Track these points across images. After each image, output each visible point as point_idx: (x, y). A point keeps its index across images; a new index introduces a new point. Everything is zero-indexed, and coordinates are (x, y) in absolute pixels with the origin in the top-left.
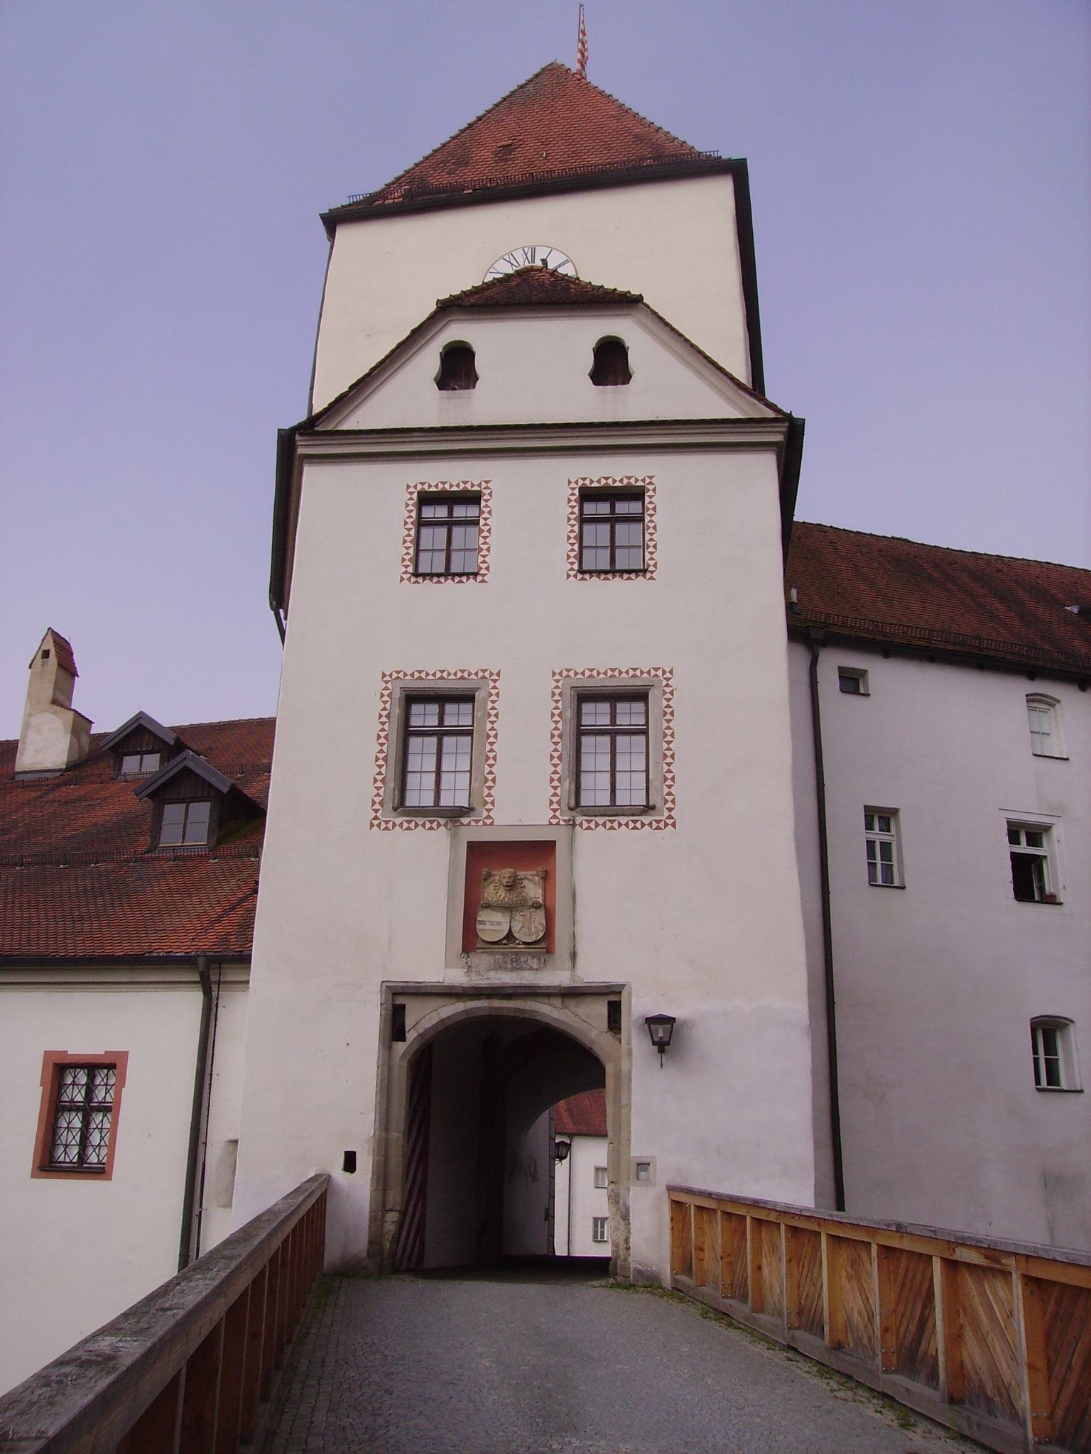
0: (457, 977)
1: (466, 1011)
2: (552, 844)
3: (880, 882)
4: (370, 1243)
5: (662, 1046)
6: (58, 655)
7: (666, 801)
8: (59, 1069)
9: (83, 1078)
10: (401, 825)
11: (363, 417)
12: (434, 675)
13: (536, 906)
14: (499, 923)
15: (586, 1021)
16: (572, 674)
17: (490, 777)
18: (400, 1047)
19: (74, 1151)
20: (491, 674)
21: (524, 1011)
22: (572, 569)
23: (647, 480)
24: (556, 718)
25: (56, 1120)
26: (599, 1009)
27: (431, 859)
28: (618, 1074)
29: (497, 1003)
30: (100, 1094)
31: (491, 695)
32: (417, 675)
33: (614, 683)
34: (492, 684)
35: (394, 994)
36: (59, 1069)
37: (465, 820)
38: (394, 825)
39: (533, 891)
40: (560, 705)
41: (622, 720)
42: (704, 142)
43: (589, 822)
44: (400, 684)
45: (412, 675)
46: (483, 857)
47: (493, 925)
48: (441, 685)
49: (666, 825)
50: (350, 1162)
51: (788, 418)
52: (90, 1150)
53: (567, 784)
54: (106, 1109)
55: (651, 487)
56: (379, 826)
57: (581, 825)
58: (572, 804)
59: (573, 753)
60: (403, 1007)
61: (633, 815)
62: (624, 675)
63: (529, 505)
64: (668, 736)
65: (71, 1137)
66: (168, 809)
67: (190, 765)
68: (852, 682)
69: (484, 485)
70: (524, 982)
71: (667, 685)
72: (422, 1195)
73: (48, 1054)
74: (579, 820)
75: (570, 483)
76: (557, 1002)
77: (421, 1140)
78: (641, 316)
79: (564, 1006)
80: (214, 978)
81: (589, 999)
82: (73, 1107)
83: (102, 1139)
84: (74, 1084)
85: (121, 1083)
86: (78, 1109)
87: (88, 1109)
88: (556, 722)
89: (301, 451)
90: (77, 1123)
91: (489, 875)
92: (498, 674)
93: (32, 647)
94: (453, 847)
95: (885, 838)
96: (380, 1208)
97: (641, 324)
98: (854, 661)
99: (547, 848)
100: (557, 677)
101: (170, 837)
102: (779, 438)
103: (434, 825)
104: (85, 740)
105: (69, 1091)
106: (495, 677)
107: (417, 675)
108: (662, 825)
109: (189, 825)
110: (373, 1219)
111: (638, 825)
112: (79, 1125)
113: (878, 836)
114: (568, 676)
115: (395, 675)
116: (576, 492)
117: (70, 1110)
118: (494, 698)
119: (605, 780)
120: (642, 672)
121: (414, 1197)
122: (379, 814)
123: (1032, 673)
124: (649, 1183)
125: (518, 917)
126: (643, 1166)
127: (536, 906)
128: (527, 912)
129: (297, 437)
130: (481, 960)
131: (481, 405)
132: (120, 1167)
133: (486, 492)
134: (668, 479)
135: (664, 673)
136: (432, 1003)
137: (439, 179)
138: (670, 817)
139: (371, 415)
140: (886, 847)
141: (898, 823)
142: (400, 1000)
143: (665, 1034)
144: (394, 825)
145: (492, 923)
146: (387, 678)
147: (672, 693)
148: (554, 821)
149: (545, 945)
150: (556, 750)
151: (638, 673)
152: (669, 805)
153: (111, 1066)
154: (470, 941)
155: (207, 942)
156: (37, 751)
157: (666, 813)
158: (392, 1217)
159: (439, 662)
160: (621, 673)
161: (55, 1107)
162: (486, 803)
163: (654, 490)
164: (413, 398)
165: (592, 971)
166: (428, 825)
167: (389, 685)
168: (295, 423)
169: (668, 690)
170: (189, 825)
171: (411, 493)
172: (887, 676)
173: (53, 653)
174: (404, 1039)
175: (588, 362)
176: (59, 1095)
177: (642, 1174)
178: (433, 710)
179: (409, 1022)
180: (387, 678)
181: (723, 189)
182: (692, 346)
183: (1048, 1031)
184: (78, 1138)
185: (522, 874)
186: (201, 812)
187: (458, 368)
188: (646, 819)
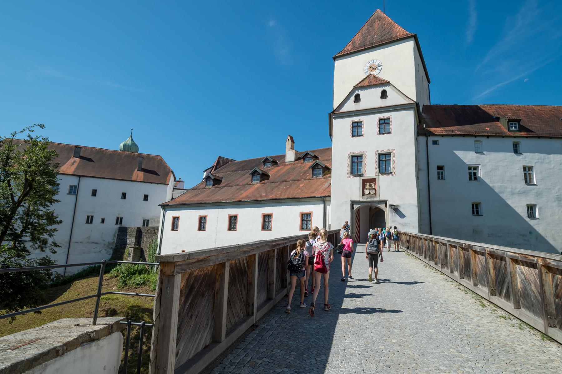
2: (375, 179)
8: (303, 215)
11: (343, 110)
15: (382, 206)
27: (357, 181)
36: (303, 215)
46: (365, 182)
54: (310, 220)
63: (370, 123)
68: (435, 143)
98: (435, 138)
99: (375, 179)
130: (365, 197)
131: (362, 106)
132: (272, 229)
139: (344, 109)
140: (442, 173)
143: (395, 209)
154: (363, 194)
159: (356, 151)
161: (302, 220)
164: (351, 106)
165: (382, 198)
175: (380, 95)
178: (356, 161)
187: (357, 99)
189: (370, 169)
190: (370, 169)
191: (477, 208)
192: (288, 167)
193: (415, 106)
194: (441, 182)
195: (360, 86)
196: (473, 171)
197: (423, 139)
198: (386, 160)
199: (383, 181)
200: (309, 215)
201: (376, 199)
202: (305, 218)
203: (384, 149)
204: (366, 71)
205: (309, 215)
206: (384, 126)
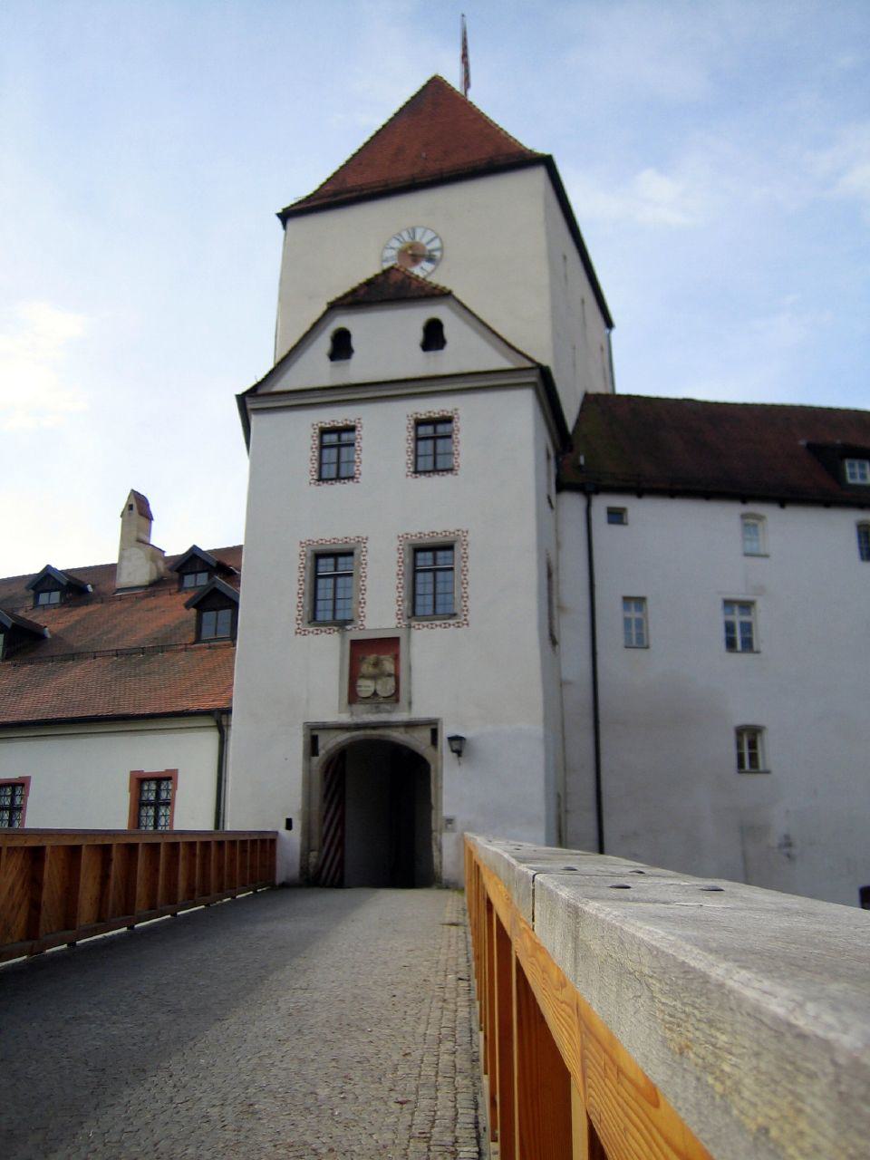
0: (345, 718)
1: (352, 738)
3: (634, 643)
4: (302, 868)
5: (459, 753)
6: (139, 508)
8: (140, 781)
9: (153, 787)
13: (390, 675)
14: (369, 687)
15: (419, 741)
18: (315, 759)
21: (384, 736)
25: (139, 812)
26: (427, 734)
27: (328, 651)
28: (436, 770)
29: (369, 732)
30: (164, 795)
33: (434, 540)
36: (140, 781)
37: (348, 627)
39: (388, 666)
42: (533, 141)
47: (366, 687)
48: (334, 547)
53: (407, 604)
58: (410, 614)
61: (445, 619)
63: (384, 433)
66: (205, 615)
67: (218, 586)
68: (616, 516)
74: (413, 623)
76: (402, 730)
77: (339, 813)
78: (452, 302)
79: (406, 733)
82: (149, 804)
85: (175, 788)
90: (151, 812)
91: (364, 658)
93: (122, 504)
94: (342, 643)
96: (306, 849)
97: (452, 309)
98: (617, 501)
102: (533, 379)
104: (161, 564)
105: (146, 794)
110: (302, 855)
112: (153, 814)
117: (147, 805)
119: (429, 600)
123: (744, 499)
124: (453, 830)
125: (380, 682)
126: (450, 821)
127: (390, 675)
128: (384, 679)
129: (247, 399)
130: (359, 708)
131: (358, 369)
134: (468, 411)
136: (333, 734)
137: (353, 180)
138: (465, 620)
140: (640, 623)
142: (316, 733)
145: (366, 686)
149: (395, 697)
153: (169, 779)
154: (353, 697)
156: (130, 574)
158: (314, 854)
159: (331, 533)
164: (316, 369)
165: (420, 712)
172: (637, 509)
175: (419, 336)
177: (449, 826)
178: (330, 566)
179: (321, 744)
181: (539, 176)
183: (749, 738)
185: (382, 657)
187: (342, 347)
188: (451, 622)
189: (380, 606)
190: (380, 606)
191: (753, 745)
193: (533, 377)
196: (737, 618)
197: (572, 504)
199: (427, 649)
200: (165, 780)
201: (400, 716)
202: (152, 791)
203: (430, 525)
205: (165, 780)
206: (432, 445)
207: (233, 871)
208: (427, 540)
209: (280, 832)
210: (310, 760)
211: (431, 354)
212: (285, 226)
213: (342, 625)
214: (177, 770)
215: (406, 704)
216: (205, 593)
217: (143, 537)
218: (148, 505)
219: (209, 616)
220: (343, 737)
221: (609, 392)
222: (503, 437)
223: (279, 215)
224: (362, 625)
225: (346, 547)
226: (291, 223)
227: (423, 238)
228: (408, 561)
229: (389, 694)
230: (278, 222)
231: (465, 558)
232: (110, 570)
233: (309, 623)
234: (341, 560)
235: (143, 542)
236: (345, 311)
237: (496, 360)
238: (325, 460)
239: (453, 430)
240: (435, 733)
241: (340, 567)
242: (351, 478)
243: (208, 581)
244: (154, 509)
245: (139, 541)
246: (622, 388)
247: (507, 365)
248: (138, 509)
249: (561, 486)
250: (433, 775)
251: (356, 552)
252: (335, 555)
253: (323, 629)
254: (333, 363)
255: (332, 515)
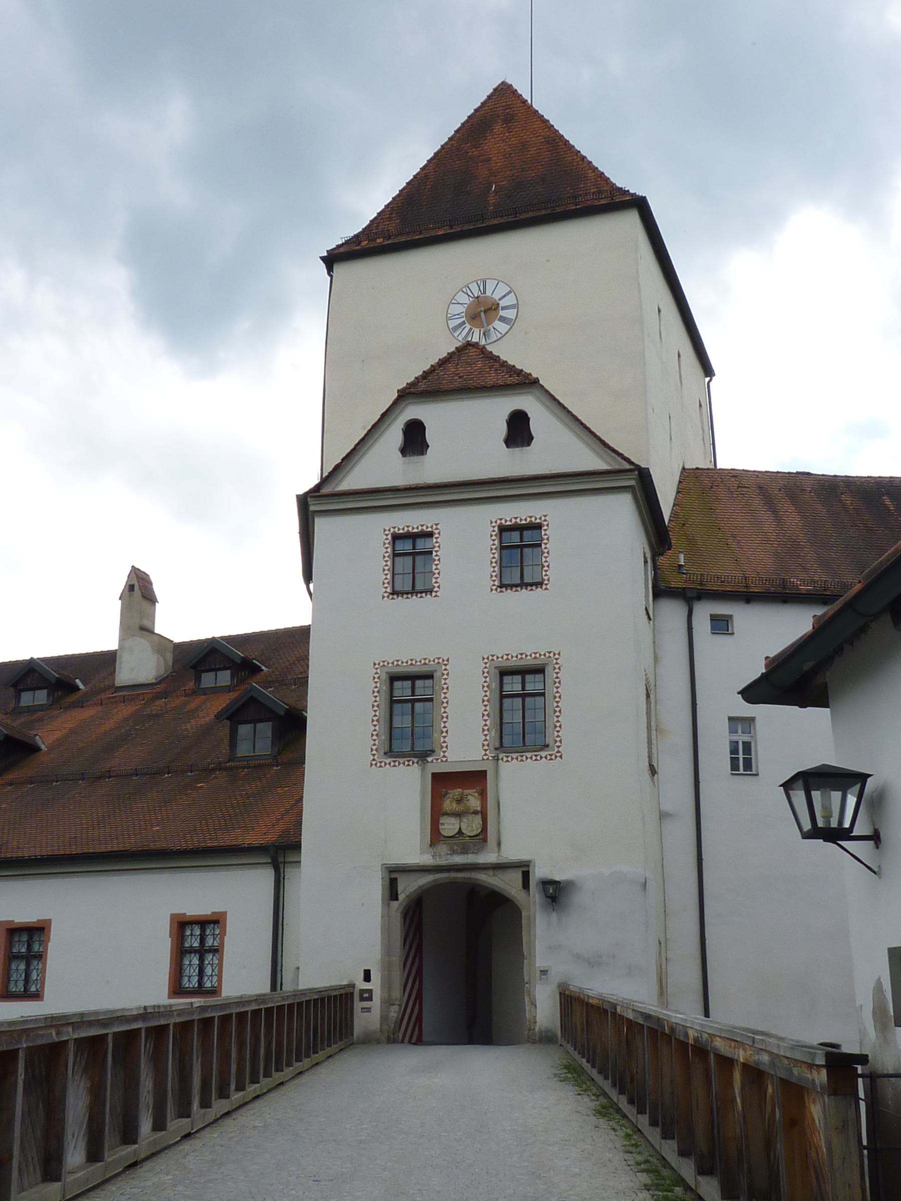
0: (427, 859)
1: (434, 881)
2: (482, 774)
7: (556, 741)
8: (181, 925)
10: (390, 764)
12: (407, 662)
13: (475, 813)
14: (453, 824)
15: (509, 885)
16: (495, 658)
17: (445, 730)
18: (395, 904)
19: (195, 979)
20: (443, 660)
21: (470, 879)
22: (494, 585)
23: (543, 518)
24: (486, 689)
25: (182, 960)
26: (517, 876)
27: (408, 783)
28: (529, 918)
30: (210, 942)
31: (443, 674)
32: (396, 663)
33: (522, 663)
34: (444, 667)
35: (390, 872)
36: (181, 925)
37: (430, 759)
38: (385, 764)
40: (488, 679)
41: (529, 687)
43: (507, 757)
44: (385, 669)
45: (393, 663)
46: (442, 782)
47: (449, 826)
49: (556, 757)
50: (367, 976)
51: (638, 468)
52: (206, 978)
53: (494, 733)
55: (545, 523)
56: (376, 765)
57: (502, 759)
58: (497, 745)
59: (498, 712)
60: (396, 879)
62: (529, 657)
63: (465, 539)
64: (557, 698)
65: (192, 971)
68: (721, 625)
69: (434, 527)
70: (469, 861)
71: (557, 663)
72: (419, 996)
73: (173, 916)
75: (491, 522)
76: (491, 872)
78: (537, 392)
79: (494, 875)
80: (281, 860)
81: (511, 870)
82: (192, 950)
83: (213, 971)
84: (191, 935)
85: (223, 933)
86: (195, 951)
87: (202, 952)
88: (486, 691)
89: (312, 508)
90: (196, 961)
92: (448, 660)
94: (423, 776)
95: (746, 738)
98: (722, 609)
99: (482, 774)
100: (486, 661)
101: (243, 750)
102: (633, 483)
103: (411, 763)
105: (189, 940)
106: (445, 662)
107: (396, 663)
108: (553, 757)
109: (256, 740)
111: (539, 758)
113: (741, 738)
114: (493, 660)
115: (382, 664)
116: (496, 529)
117: (190, 952)
118: (445, 677)
120: (540, 655)
121: (413, 998)
122: (376, 757)
126: (544, 972)
127: (475, 813)
128: (471, 817)
129: (309, 499)
130: (443, 848)
131: (433, 468)
133: (436, 531)
134: (558, 517)
135: (554, 654)
140: (747, 747)
141: (755, 728)
142: (394, 876)
143: (556, 893)
144: (385, 764)
146: (377, 666)
147: (559, 668)
148: (485, 757)
150: (486, 710)
151: (538, 655)
152: (558, 744)
153: (216, 922)
154: (436, 837)
155: (271, 838)
157: (556, 749)
159: (409, 654)
160: (526, 656)
161: (180, 952)
162: (442, 747)
163: (548, 525)
164: (385, 466)
165: (512, 852)
166: (407, 763)
167: (378, 671)
168: (306, 489)
169: (557, 666)
170: (256, 740)
171: (387, 535)
173: (136, 588)
174: (397, 899)
175: (502, 430)
176: (182, 943)
178: (408, 693)
180: (377, 666)
181: (631, 220)
182: (573, 416)
184: (197, 971)
186: (265, 729)
187: (415, 440)
188: (543, 754)
189: (464, 737)
190: (464, 737)
192: (126, 710)
194: (744, 783)
195: (431, 386)
197: (672, 613)
198: (523, 696)
201: (488, 857)
202: (196, 939)
203: (520, 647)
204: (453, 323)
206: (519, 554)
207: (304, 1029)
208: (514, 662)
209: (357, 984)
210: (389, 905)
211: (517, 450)
212: (330, 270)
213: (423, 756)
214: (226, 912)
215: (495, 843)
216: (237, 705)
217: (146, 623)
218: (151, 584)
219: (244, 730)
220: (426, 880)
221: (712, 467)
222: (597, 542)
223: (322, 258)
224: (444, 756)
225: (425, 669)
226: (338, 269)
227: (495, 292)
228: (495, 685)
229: (475, 833)
230: (323, 266)
231: (557, 682)
232: (104, 662)
233: (385, 753)
234: (419, 683)
235: (147, 630)
236: (414, 401)
237: (590, 460)
238: (396, 572)
239: (542, 540)
240: (526, 876)
241: (417, 692)
242: (429, 591)
243: (250, 691)
244: (158, 589)
245: (142, 628)
246: (725, 462)
247: (601, 465)
248: (139, 591)
249: (660, 592)
250: (524, 922)
251: (437, 675)
252: (413, 678)
253: (401, 761)
254: (407, 459)
255: (410, 633)
